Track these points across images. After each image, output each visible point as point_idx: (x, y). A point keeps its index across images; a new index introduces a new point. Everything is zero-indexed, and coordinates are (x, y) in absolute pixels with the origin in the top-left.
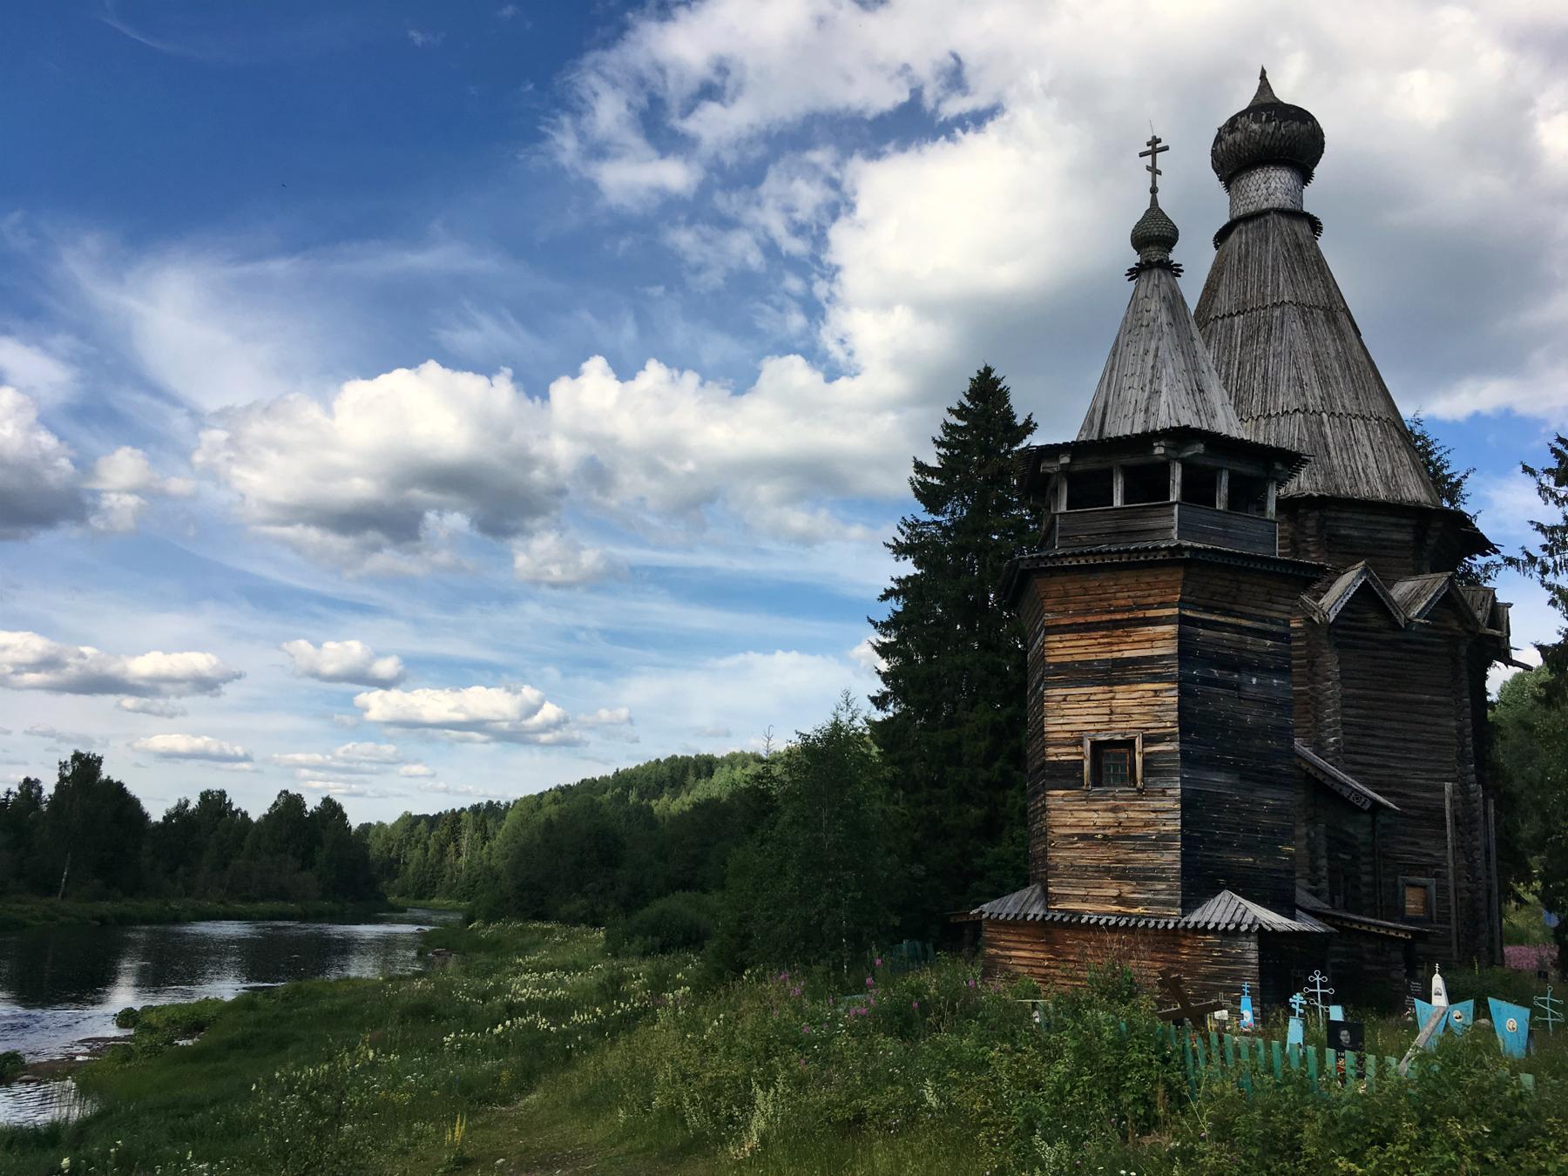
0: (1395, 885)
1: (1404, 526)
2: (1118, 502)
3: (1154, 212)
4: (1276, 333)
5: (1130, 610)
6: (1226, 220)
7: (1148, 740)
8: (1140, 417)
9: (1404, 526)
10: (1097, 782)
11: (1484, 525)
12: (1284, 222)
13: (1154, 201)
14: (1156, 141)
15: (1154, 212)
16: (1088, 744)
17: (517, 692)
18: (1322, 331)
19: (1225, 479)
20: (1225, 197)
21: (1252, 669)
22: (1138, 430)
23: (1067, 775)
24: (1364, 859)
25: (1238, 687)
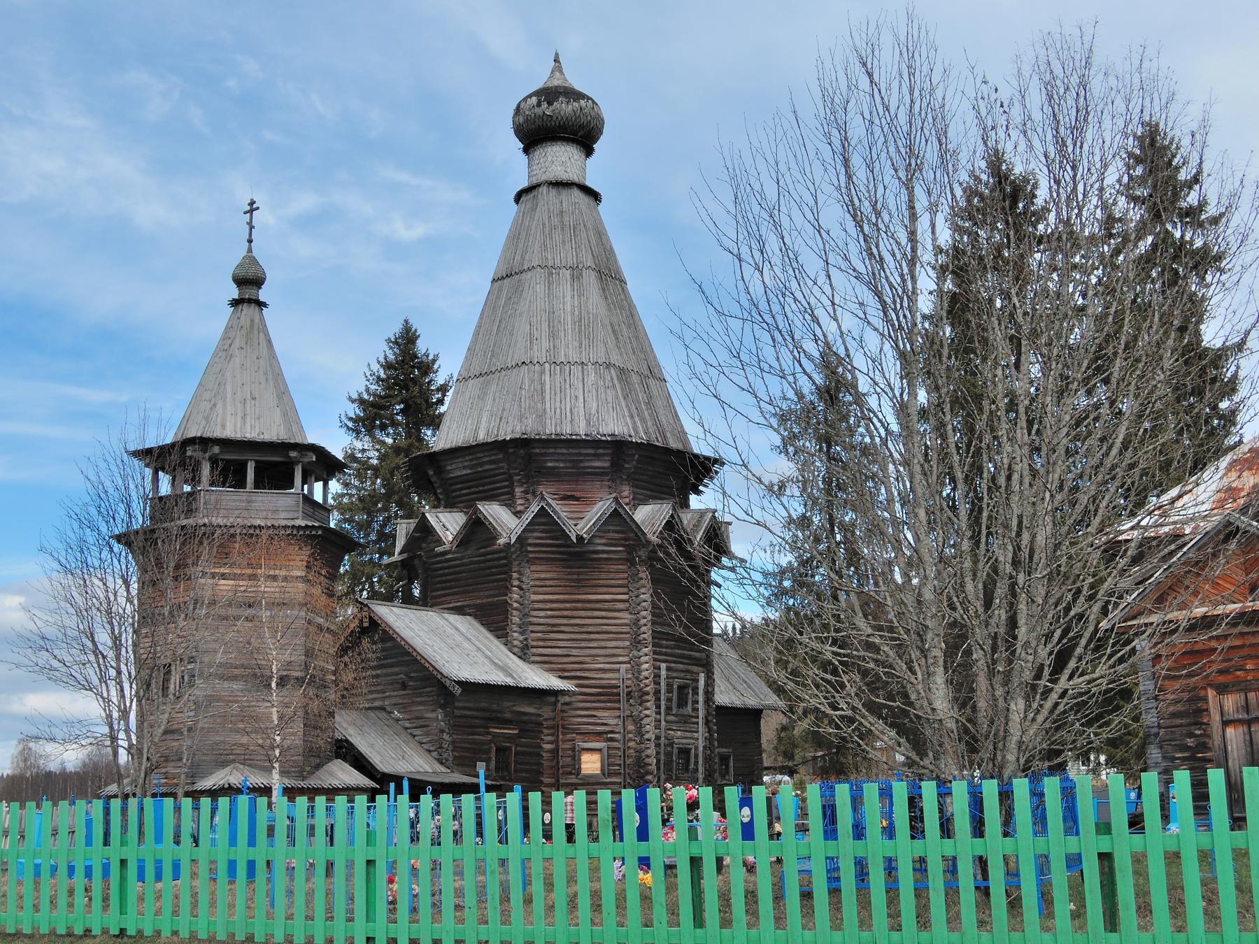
0: (573, 749)
1: (603, 455)
3: (250, 259)
4: (525, 294)
9: (603, 455)
11: (700, 447)
12: (553, 192)
13: (250, 250)
14: (252, 203)
15: (250, 259)
18: (565, 287)
24: (545, 731)
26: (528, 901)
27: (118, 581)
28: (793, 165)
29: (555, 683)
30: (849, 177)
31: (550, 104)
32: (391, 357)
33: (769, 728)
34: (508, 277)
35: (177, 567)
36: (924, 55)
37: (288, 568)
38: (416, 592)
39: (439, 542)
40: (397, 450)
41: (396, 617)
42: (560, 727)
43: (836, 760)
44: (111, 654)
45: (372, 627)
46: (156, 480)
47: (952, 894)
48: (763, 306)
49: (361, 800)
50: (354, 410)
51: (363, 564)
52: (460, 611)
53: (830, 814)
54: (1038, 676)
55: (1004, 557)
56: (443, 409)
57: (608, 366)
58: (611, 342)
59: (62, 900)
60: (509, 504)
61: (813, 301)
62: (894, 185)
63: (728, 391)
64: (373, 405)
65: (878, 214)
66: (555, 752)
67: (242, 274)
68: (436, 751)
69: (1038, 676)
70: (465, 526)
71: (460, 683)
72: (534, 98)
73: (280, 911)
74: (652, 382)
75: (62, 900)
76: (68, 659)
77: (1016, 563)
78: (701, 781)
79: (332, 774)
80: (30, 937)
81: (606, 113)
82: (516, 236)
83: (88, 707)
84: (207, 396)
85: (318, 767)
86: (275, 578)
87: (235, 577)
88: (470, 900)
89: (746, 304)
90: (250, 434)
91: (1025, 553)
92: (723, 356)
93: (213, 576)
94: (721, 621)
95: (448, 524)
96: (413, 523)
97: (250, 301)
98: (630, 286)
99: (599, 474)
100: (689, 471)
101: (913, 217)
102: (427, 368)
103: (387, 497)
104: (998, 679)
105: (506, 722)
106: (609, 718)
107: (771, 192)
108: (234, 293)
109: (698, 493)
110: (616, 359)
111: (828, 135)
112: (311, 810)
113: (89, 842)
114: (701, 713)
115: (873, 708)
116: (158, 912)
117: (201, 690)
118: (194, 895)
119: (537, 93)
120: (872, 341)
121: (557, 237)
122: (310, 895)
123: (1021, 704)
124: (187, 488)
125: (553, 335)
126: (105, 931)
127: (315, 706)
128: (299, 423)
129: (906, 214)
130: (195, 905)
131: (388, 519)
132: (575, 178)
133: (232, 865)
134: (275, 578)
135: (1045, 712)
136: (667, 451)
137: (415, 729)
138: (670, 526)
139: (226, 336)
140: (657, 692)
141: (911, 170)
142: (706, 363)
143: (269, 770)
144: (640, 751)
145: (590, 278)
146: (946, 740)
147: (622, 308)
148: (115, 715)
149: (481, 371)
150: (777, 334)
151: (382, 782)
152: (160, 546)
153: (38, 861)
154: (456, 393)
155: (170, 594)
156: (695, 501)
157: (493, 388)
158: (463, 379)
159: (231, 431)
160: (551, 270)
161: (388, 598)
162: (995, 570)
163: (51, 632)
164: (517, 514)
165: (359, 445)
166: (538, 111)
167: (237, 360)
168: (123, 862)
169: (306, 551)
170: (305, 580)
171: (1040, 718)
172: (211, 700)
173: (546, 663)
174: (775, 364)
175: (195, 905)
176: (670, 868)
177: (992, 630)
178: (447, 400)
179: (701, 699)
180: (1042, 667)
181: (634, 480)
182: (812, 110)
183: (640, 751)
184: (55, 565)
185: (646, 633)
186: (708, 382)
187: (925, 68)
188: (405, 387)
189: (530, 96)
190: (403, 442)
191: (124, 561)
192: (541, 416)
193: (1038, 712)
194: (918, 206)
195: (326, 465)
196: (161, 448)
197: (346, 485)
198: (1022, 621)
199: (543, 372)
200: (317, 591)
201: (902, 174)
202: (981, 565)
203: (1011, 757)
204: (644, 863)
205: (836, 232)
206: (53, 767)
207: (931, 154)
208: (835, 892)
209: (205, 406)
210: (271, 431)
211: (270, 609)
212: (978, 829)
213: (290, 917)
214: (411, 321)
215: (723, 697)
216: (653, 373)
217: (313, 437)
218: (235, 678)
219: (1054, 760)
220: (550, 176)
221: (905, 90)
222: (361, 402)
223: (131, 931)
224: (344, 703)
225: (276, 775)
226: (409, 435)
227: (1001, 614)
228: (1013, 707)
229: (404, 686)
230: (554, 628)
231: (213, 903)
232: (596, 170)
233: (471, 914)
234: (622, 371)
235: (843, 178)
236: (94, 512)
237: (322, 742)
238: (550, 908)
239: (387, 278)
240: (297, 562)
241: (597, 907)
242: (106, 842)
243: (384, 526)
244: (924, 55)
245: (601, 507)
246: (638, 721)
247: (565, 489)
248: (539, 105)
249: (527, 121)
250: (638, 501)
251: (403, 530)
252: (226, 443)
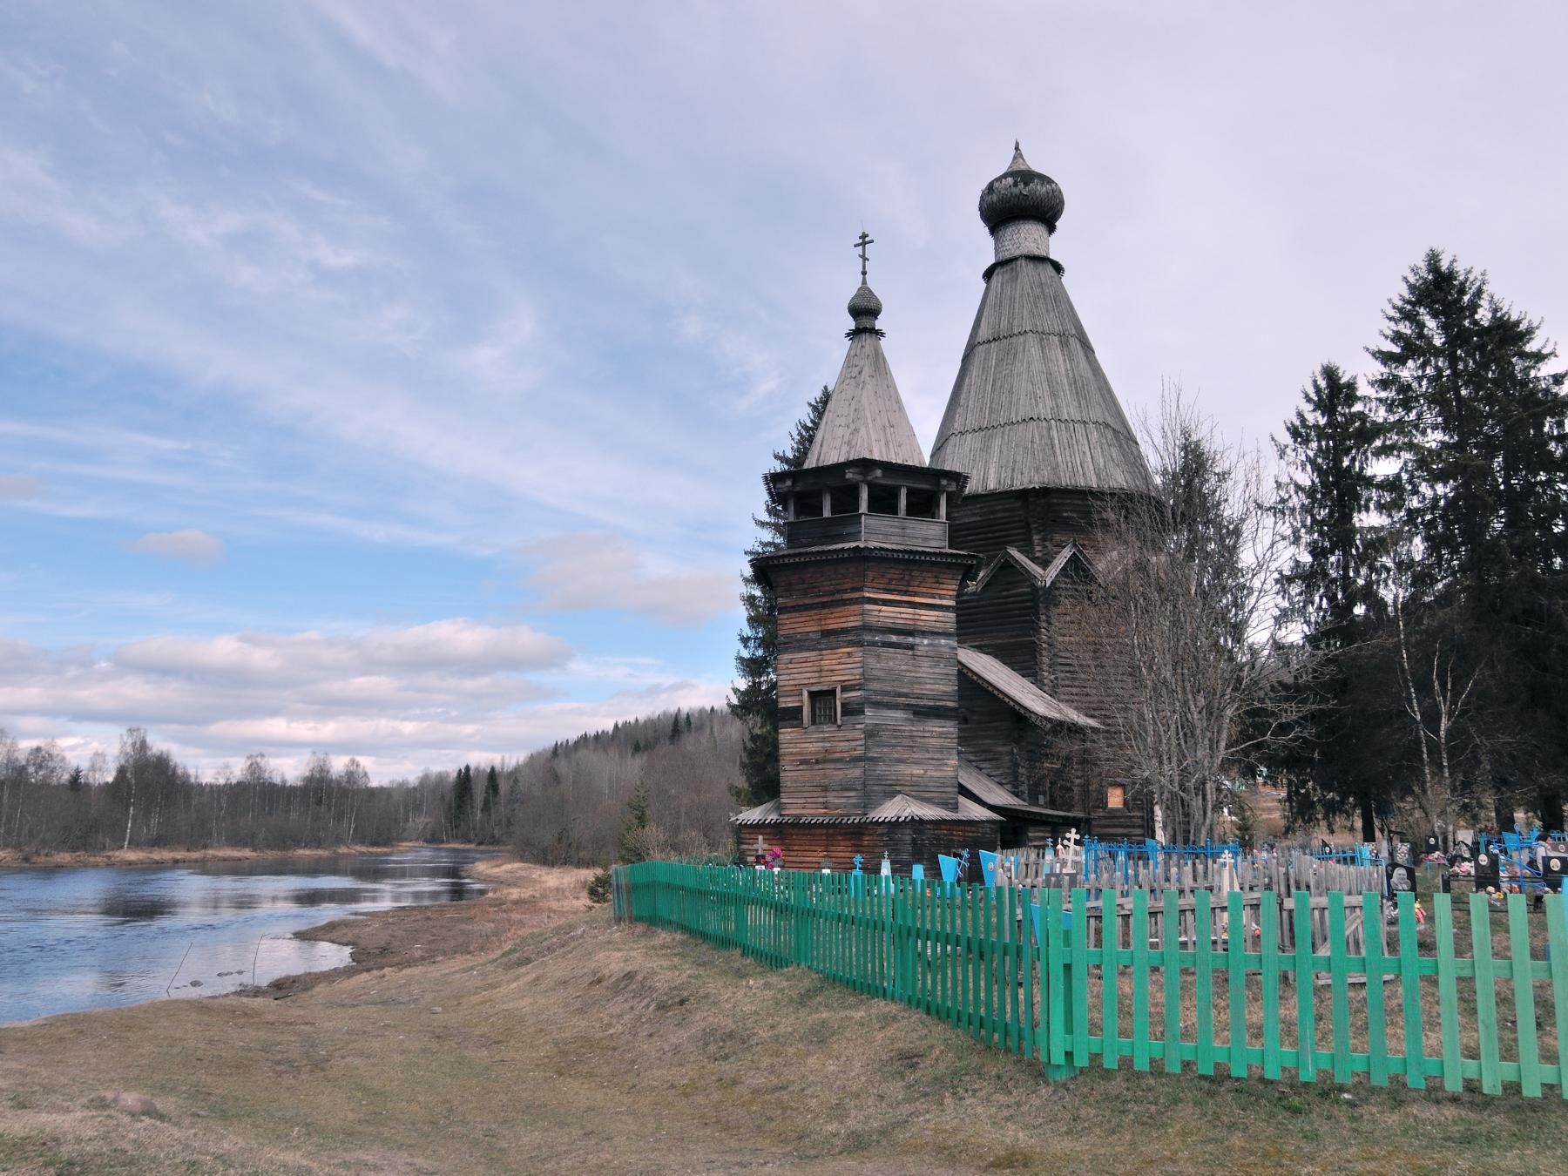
2: (827, 513)
3: (865, 291)
4: (1020, 355)
5: (833, 594)
6: (991, 260)
7: (844, 689)
8: (845, 448)
10: (814, 722)
12: (1031, 265)
13: (864, 282)
14: (864, 236)
15: (865, 291)
16: (806, 694)
17: (1399, 456)
18: (1056, 353)
19: (903, 492)
20: (990, 241)
21: (924, 634)
22: (842, 460)
23: (794, 715)
25: (911, 647)
29: (1082, 720)
31: (1026, 184)
72: (1010, 180)
108: (851, 324)
121: (1041, 305)
125: (1054, 395)
157: (998, 441)
160: (1042, 335)
166: (1015, 190)
167: (870, 388)
189: (1005, 176)
192: (1055, 468)
199: (1049, 429)
214: (1507, 291)
220: (1025, 251)
248: (1015, 184)
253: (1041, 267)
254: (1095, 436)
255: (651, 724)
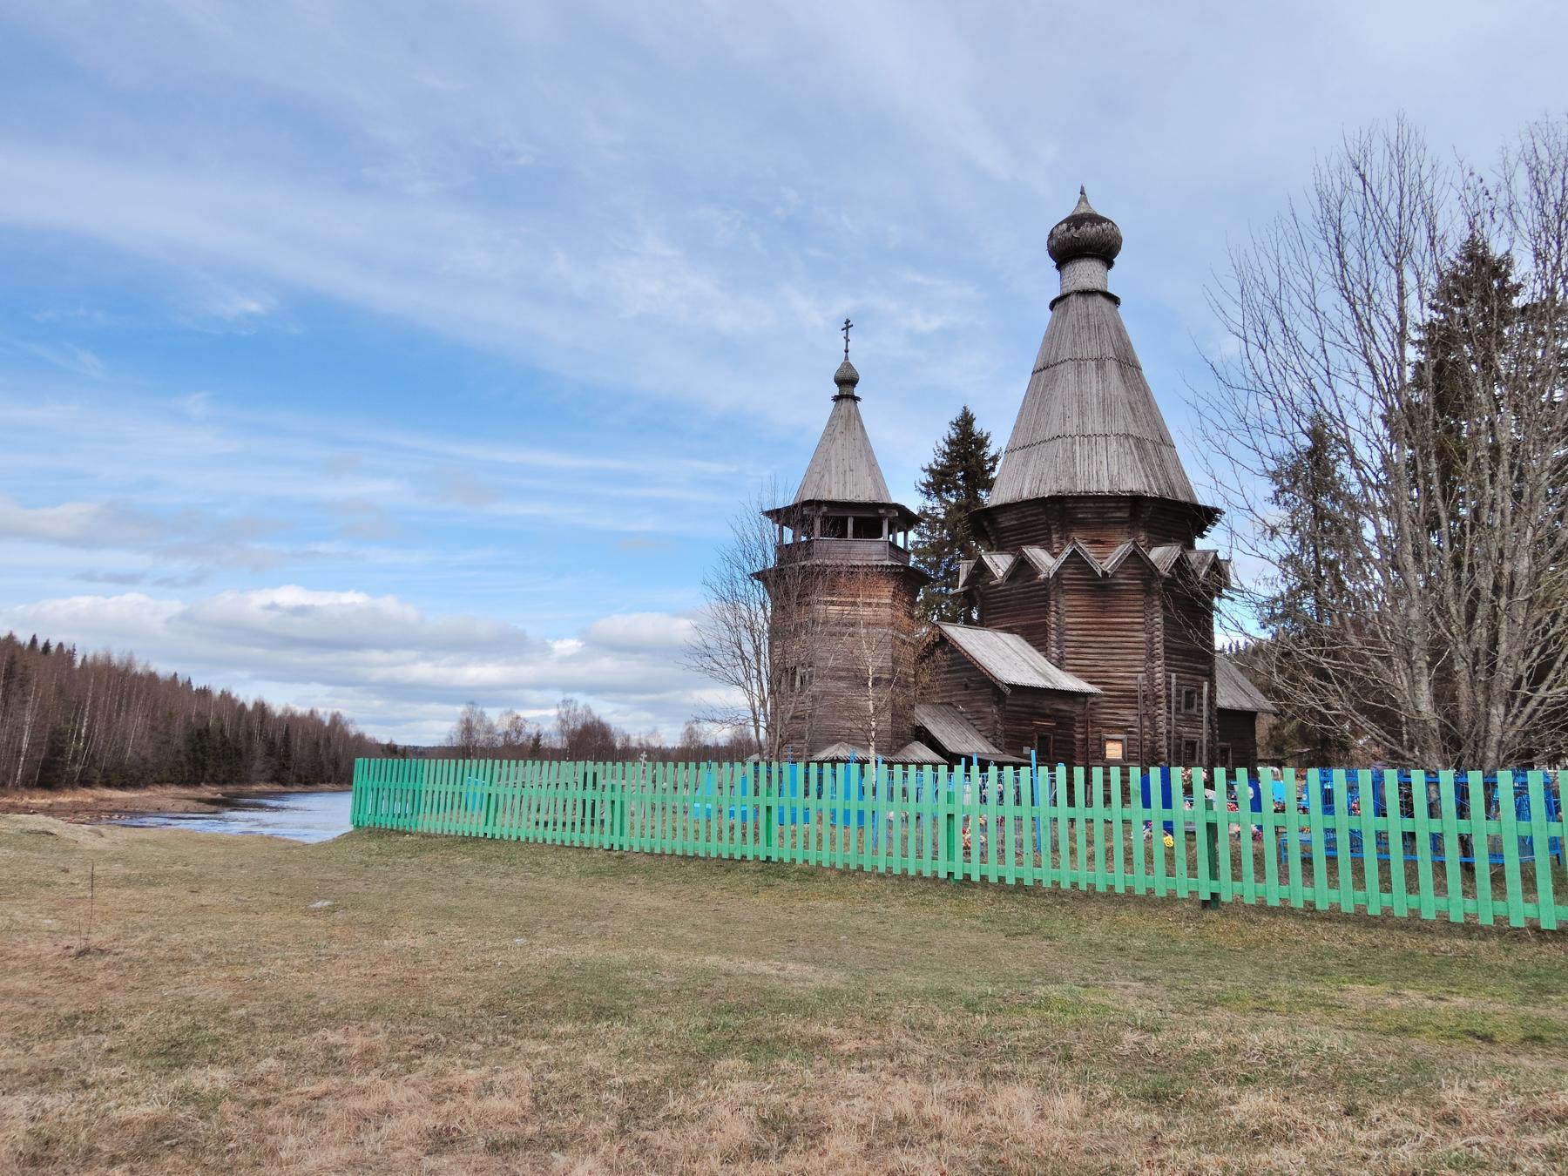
3: (847, 365)
6: (1058, 295)
11: (1204, 498)
12: (1081, 299)
15: (847, 365)
26: (1073, 852)
27: (758, 606)
28: (1292, 260)
29: (1085, 687)
30: (1343, 265)
31: (1077, 228)
32: (954, 436)
33: (1263, 727)
34: (1045, 369)
35: (799, 596)
36: (1413, 155)
37: (879, 597)
38: (975, 616)
39: (993, 577)
40: (958, 507)
41: (961, 635)
42: (1089, 722)
43: (1321, 749)
44: (754, 660)
45: (943, 641)
46: (781, 530)
47: (1440, 868)
48: (1267, 379)
49: (928, 769)
50: (926, 478)
51: (934, 595)
52: (1009, 630)
53: (1328, 797)
54: (1517, 685)
55: (1485, 584)
56: (994, 475)
57: (1127, 436)
58: (1129, 416)
59: (726, 834)
60: (1047, 547)
61: (1310, 373)
62: (1384, 269)
63: (1236, 450)
64: (940, 473)
65: (1370, 298)
66: (1085, 740)
67: (841, 376)
68: (992, 737)
69: (1517, 685)
70: (1012, 565)
71: (1009, 685)
73: (882, 849)
74: (1163, 448)
75: (726, 834)
76: (724, 663)
77: (1497, 589)
78: (259, 747)
79: (913, 752)
80: (704, 859)
81: (1123, 234)
82: (1052, 336)
83: (737, 699)
84: (817, 469)
85: (903, 746)
86: (870, 604)
87: (841, 603)
88: (1028, 847)
89: (1251, 377)
90: (850, 497)
91: (1505, 582)
92: (1232, 420)
93: (826, 603)
94: (1221, 640)
95: (999, 564)
96: (972, 562)
97: (847, 397)
98: (1145, 372)
99: (1120, 523)
100: (1204, 517)
101: (1402, 296)
102: (981, 443)
103: (952, 544)
104: (1480, 687)
105: (1045, 717)
106: (1129, 716)
107: (1273, 284)
108: (836, 391)
109: (1202, 536)
110: (1133, 430)
111: (1324, 231)
112: (891, 777)
113: (744, 793)
114: (1205, 714)
115: (1364, 710)
116: (794, 846)
117: (816, 687)
118: (819, 835)
119: (1067, 221)
120: (1363, 403)
121: (1085, 335)
122: (905, 838)
123: (1502, 709)
124: (804, 539)
125: (1082, 414)
126: (756, 858)
127: (900, 700)
128: (885, 488)
129: (1395, 291)
130: (820, 842)
131: (952, 561)
132: (1097, 285)
133: (847, 813)
134: (870, 604)
135: (1524, 717)
136: (1177, 503)
137: (975, 720)
138: (1180, 563)
139: (830, 424)
140: (1169, 696)
141: (1401, 255)
142: (1217, 426)
143: (867, 748)
144: (1154, 743)
145: (1112, 368)
146: (1430, 738)
147: (1138, 389)
148: (757, 704)
149: (1023, 445)
150: (1279, 402)
151: (952, 759)
152: (787, 582)
153: (709, 806)
154: (1005, 462)
155: (795, 616)
156: (1200, 544)
158: (1010, 451)
159: (835, 495)
160: (1079, 362)
161: (954, 620)
162: (1477, 593)
163: (712, 643)
164: (1055, 555)
165: (929, 504)
168: (769, 809)
169: (893, 584)
170: (892, 606)
171: (1519, 722)
172: (825, 694)
173: (1078, 671)
174: (1277, 426)
175: (820, 842)
176: (1191, 835)
177: (1473, 646)
178: (998, 468)
179: (1205, 702)
180: (1520, 680)
181: (1148, 527)
182: (1309, 210)
183: (1154, 743)
184: (714, 595)
185: (1159, 649)
186: (1219, 442)
187: (1415, 167)
188: (965, 458)
190: (964, 501)
191: (758, 592)
192: (1073, 478)
193: (1516, 716)
194: (1407, 287)
195: (906, 519)
196: (787, 508)
197: (920, 534)
198: (1502, 638)
200: (901, 614)
201: (1393, 260)
202: (1463, 591)
203: (1491, 755)
204: (1168, 828)
205: (1333, 315)
206: (710, 742)
207: (1420, 239)
208: (1332, 860)
209: (816, 477)
210: (865, 494)
211: (865, 627)
212: (1463, 811)
213: (889, 854)
215: (1225, 700)
216: (1164, 441)
217: (895, 499)
218: (841, 678)
219: (1523, 760)
220: (1078, 287)
221: (1395, 187)
222: (931, 471)
223: (774, 859)
224: (923, 698)
225: (872, 751)
226: (968, 496)
227: (1481, 633)
228: (1494, 711)
229: (967, 687)
230: (1084, 645)
231: (833, 842)
232: (1116, 279)
233: (1028, 859)
234: (1139, 442)
235: (1337, 267)
236: (740, 555)
237: (906, 728)
238: (1091, 858)
239: (949, 374)
240: (885, 593)
241: (1128, 860)
242: (756, 793)
243: (949, 566)
244: (1413, 155)
245: (1121, 549)
246: (1152, 719)
247: (1093, 534)
248: (1068, 229)
249: (1058, 243)
250: (1153, 544)
251: (964, 568)
252: (832, 504)
253: (1090, 300)
254: (1114, 446)
255: (120, 684)
